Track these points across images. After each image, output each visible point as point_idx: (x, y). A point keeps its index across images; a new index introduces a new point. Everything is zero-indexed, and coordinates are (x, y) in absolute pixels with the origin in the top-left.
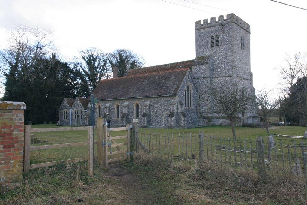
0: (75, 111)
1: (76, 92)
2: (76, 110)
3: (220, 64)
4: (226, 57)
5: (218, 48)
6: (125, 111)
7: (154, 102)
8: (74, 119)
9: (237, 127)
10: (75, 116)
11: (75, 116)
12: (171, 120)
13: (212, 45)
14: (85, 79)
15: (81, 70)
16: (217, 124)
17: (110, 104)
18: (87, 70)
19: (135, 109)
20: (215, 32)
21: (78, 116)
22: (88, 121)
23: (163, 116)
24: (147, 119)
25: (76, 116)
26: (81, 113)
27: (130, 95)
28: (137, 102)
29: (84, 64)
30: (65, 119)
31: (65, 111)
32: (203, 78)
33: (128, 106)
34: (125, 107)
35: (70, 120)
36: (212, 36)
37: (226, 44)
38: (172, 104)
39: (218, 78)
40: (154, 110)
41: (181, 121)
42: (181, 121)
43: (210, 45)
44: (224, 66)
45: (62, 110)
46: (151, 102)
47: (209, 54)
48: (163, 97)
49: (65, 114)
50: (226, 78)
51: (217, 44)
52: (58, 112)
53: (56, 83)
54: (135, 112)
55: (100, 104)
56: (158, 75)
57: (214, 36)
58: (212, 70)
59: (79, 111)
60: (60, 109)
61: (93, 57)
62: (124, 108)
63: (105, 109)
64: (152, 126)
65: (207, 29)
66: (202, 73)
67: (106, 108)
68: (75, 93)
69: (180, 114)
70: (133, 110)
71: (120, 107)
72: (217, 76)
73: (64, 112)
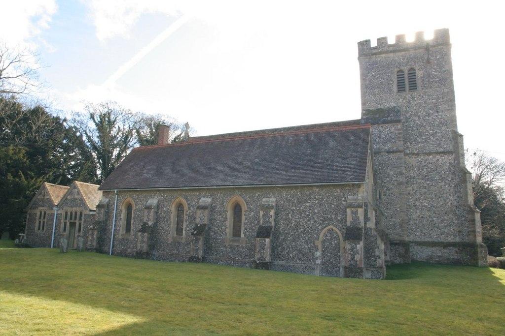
0: (66, 213)
1: (71, 174)
2: (69, 210)
3: (422, 126)
4: (438, 112)
5: (415, 93)
6: (202, 218)
7: (289, 201)
8: (62, 230)
9: (480, 267)
10: (65, 223)
11: (65, 223)
12: (352, 249)
13: (401, 88)
14: (91, 156)
15: (84, 138)
16: (419, 259)
17: (159, 201)
18: (96, 139)
19: (230, 214)
20: (408, 62)
21: (73, 225)
22: (98, 238)
23: (318, 236)
24: (272, 242)
25: (68, 224)
26: (80, 219)
27: (216, 181)
28: (237, 197)
29: (92, 126)
30: (39, 229)
31: (41, 212)
32: (389, 152)
33: (211, 208)
34: (203, 208)
35: (52, 232)
36: (401, 71)
37: (436, 85)
38: (350, 206)
39: (418, 154)
40: (290, 221)
41: (377, 253)
42: (377, 253)
43: (395, 88)
44: (433, 130)
45: (36, 208)
46: (281, 199)
47: (393, 105)
48: (317, 186)
49: (40, 218)
50: (438, 157)
51: (413, 86)
52: (26, 212)
53: (52, 334)
54: (229, 222)
55: (133, 198)
56: (286, 138)
57: (406, 69)
58: (406, 139)
59: (76, 213)
60: (30, 205)
61: (109, 118)
62: (199, 212)
63: (146, 212)
64: (281, 262)
65: (386, 55)
66: (385, 143)
67: (148, 208)
68: (69, 176)
69: (374, 233)
70: (226, 219)
71: (186, 208)
72: (416, 152)
73: (39, 214)
